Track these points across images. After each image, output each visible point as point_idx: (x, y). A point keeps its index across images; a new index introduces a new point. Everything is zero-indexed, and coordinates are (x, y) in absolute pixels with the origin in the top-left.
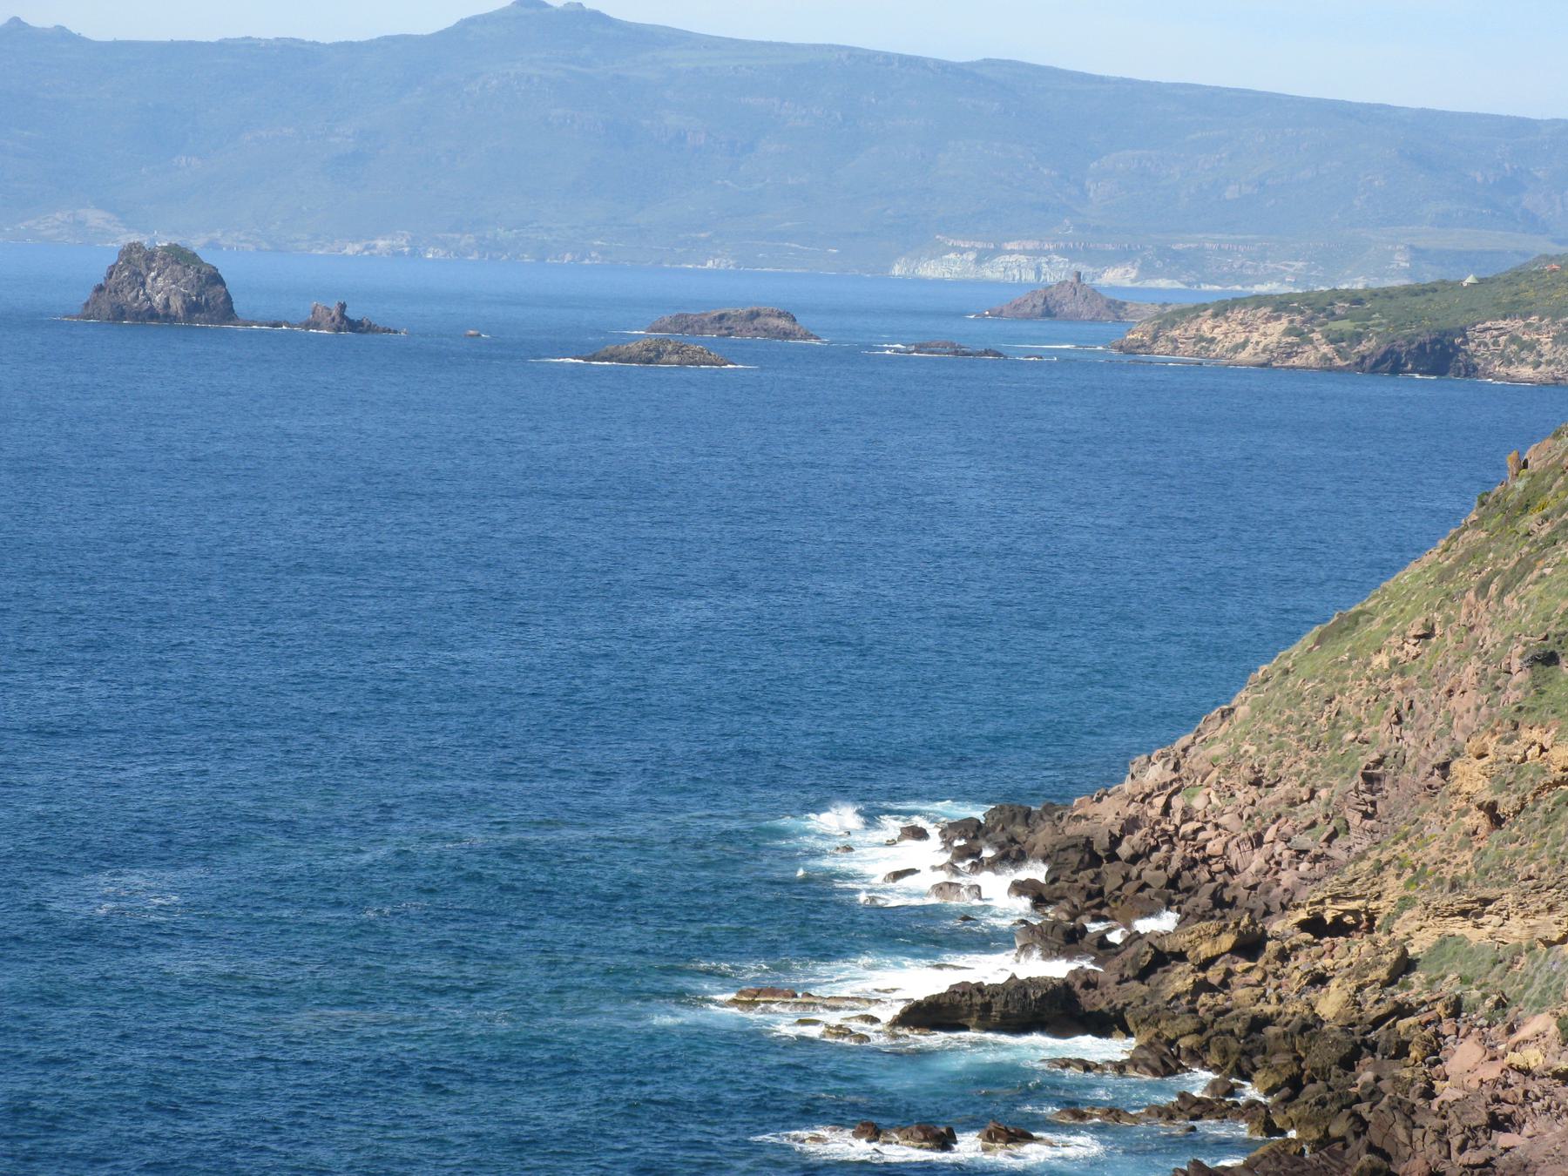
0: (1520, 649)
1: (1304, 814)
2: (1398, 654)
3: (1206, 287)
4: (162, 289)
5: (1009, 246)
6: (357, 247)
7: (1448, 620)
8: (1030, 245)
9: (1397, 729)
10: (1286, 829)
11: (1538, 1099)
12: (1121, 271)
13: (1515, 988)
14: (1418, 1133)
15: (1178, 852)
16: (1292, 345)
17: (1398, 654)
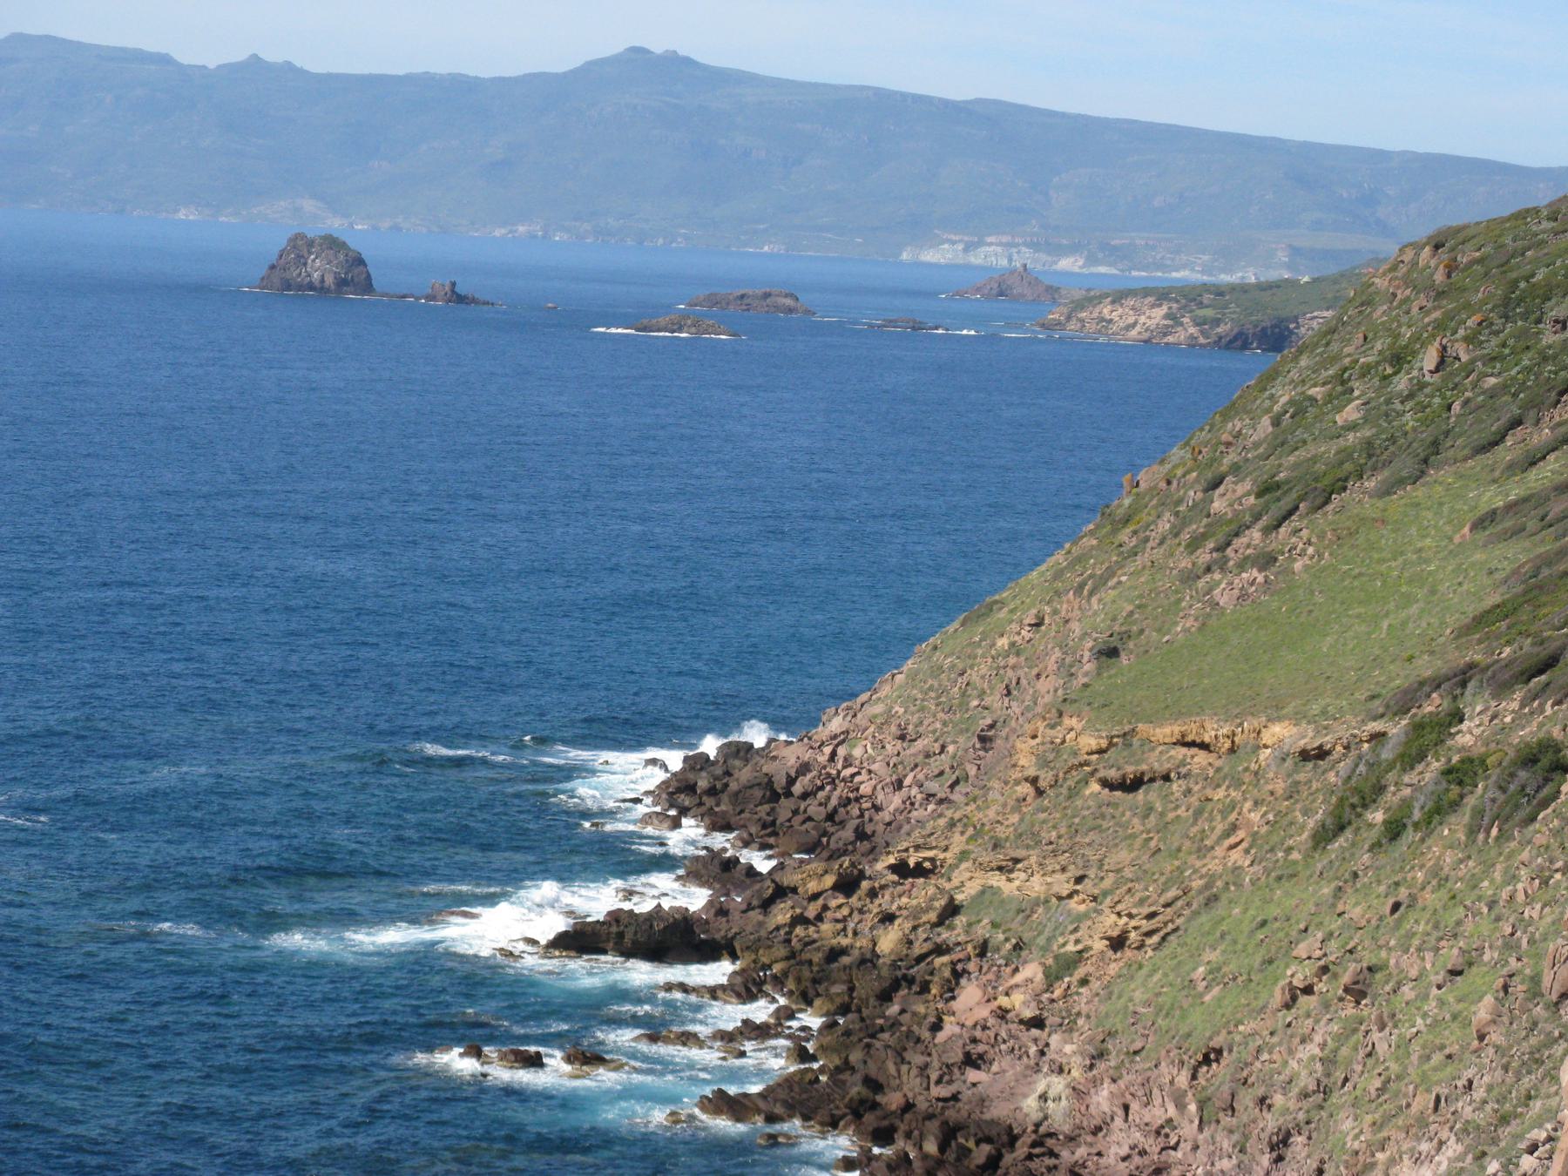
0: (1090, 644)
1: (936, 764)
2: (1017, 638)
3: (1134, 273)
4: (319, 268)
5: (989, 240)
6: (503, 231)
7: (1055, 612)
8: (1005, 239)
9: (1006, 700)
10: (921, 776)
11: (1004, 1042)
12: (1072, 260)
13: (1031, 934)
14: (904, 1068)
15: (836, 793)
16: (1167, 326)
17: (1017, 638)
